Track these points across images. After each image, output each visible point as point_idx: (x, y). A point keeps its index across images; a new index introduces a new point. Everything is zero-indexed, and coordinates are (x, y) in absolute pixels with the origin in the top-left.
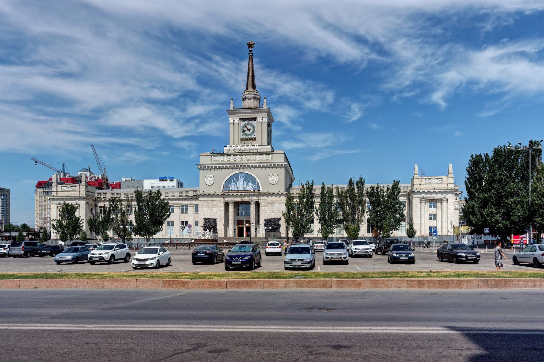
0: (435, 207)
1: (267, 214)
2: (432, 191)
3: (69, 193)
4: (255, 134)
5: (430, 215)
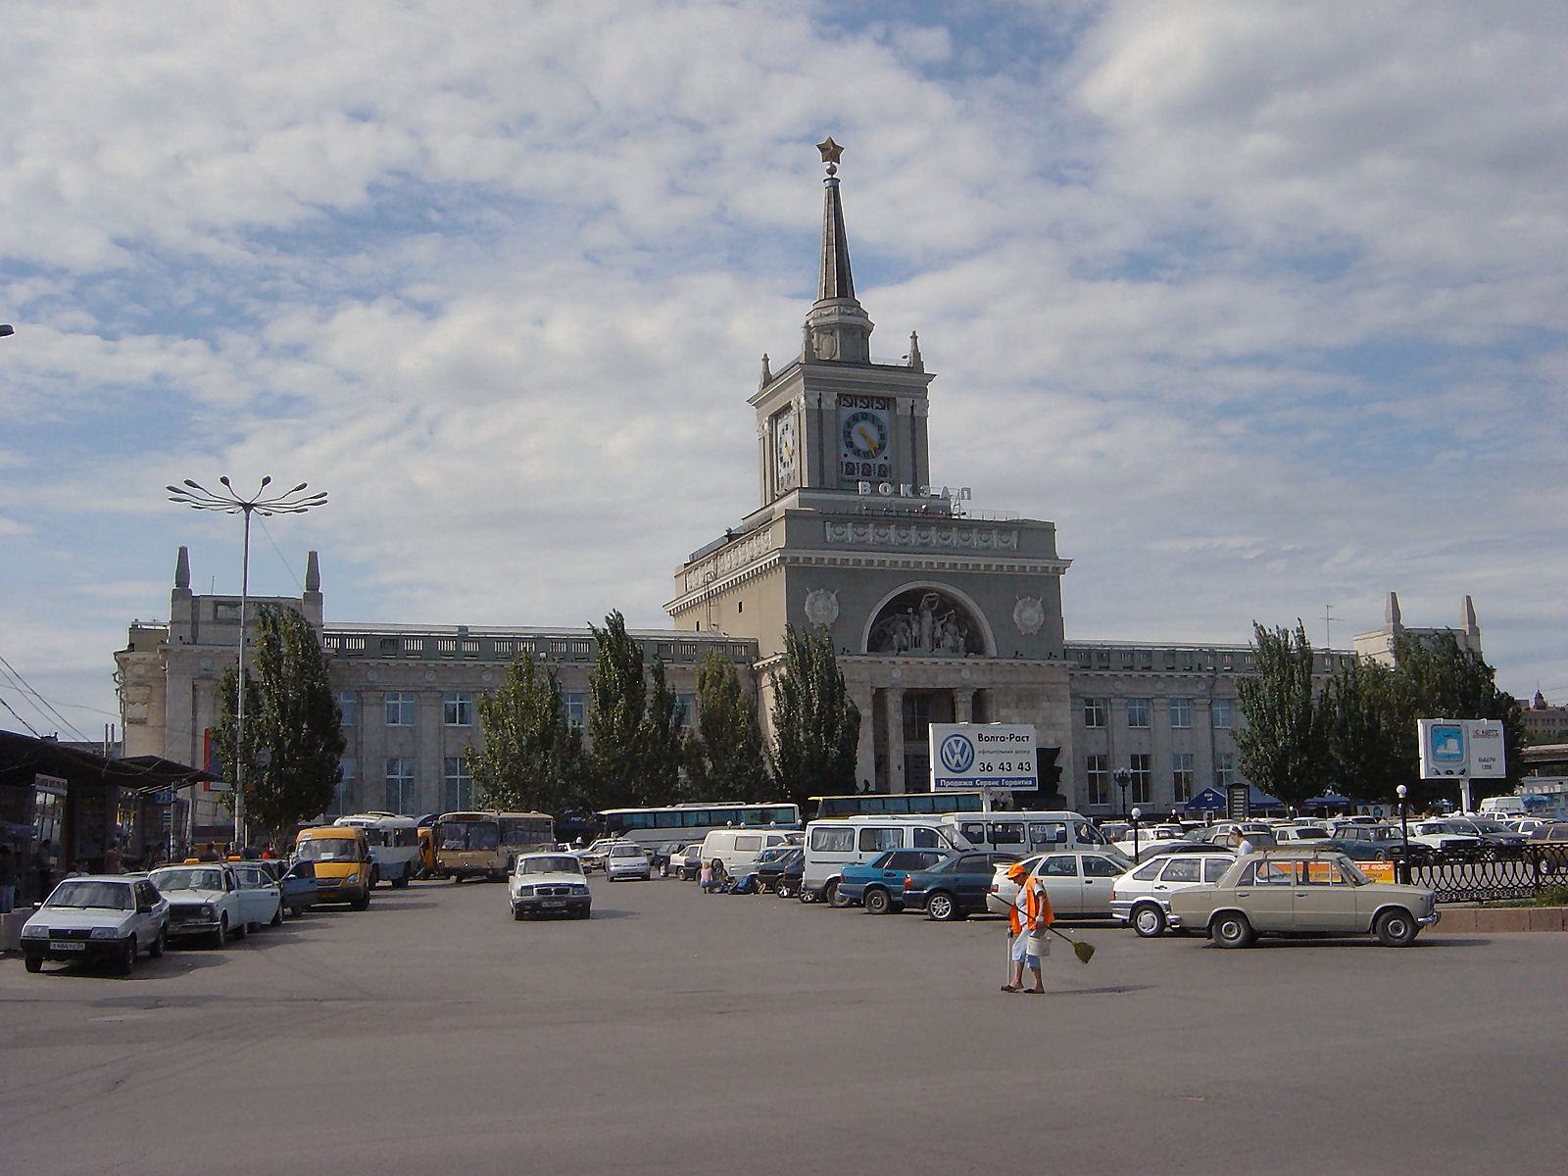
4: (887, 452)
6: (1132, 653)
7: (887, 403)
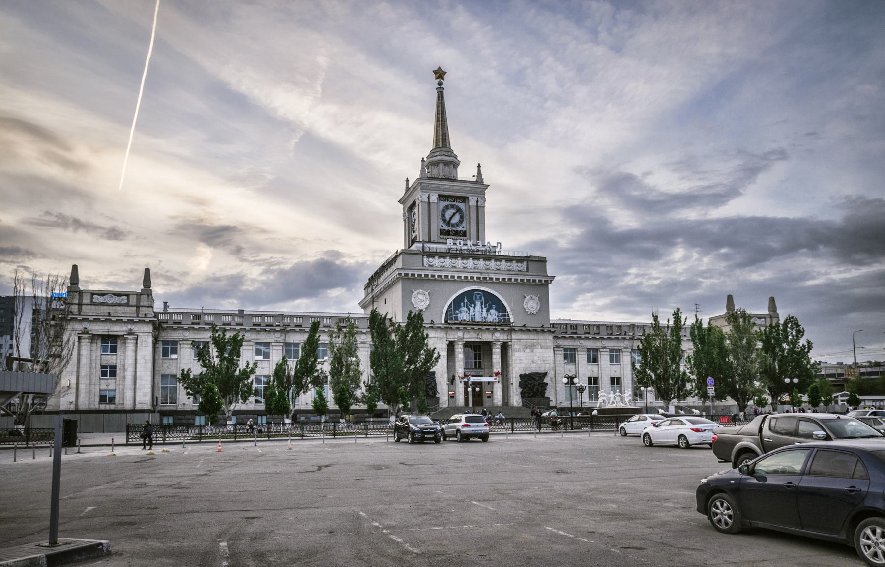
0: (114, 350)
1: (523, 365)
2: (539, 329)
3: (110, 309)
4: (464, 224)
5: (103, 366)
6: (589, 325)
7: (464, 199)
